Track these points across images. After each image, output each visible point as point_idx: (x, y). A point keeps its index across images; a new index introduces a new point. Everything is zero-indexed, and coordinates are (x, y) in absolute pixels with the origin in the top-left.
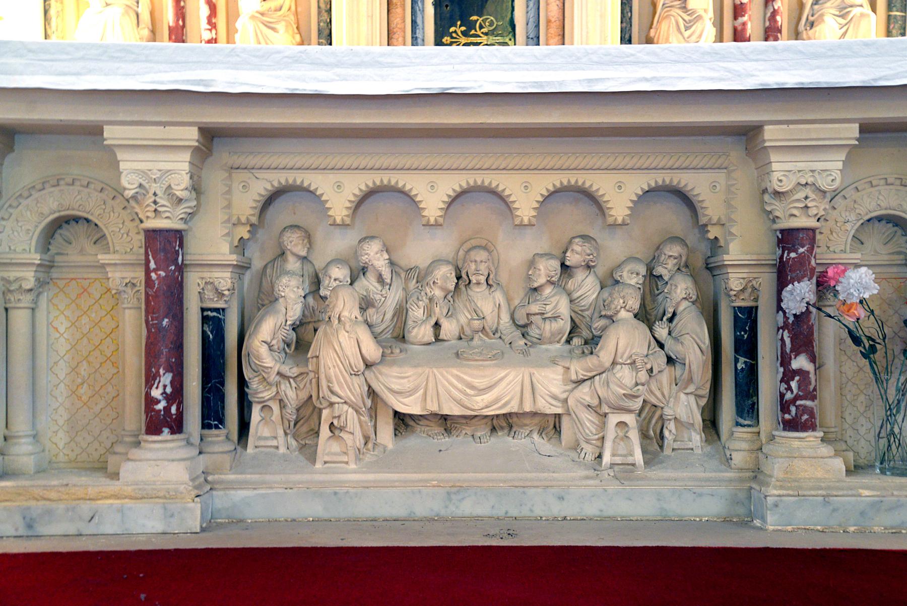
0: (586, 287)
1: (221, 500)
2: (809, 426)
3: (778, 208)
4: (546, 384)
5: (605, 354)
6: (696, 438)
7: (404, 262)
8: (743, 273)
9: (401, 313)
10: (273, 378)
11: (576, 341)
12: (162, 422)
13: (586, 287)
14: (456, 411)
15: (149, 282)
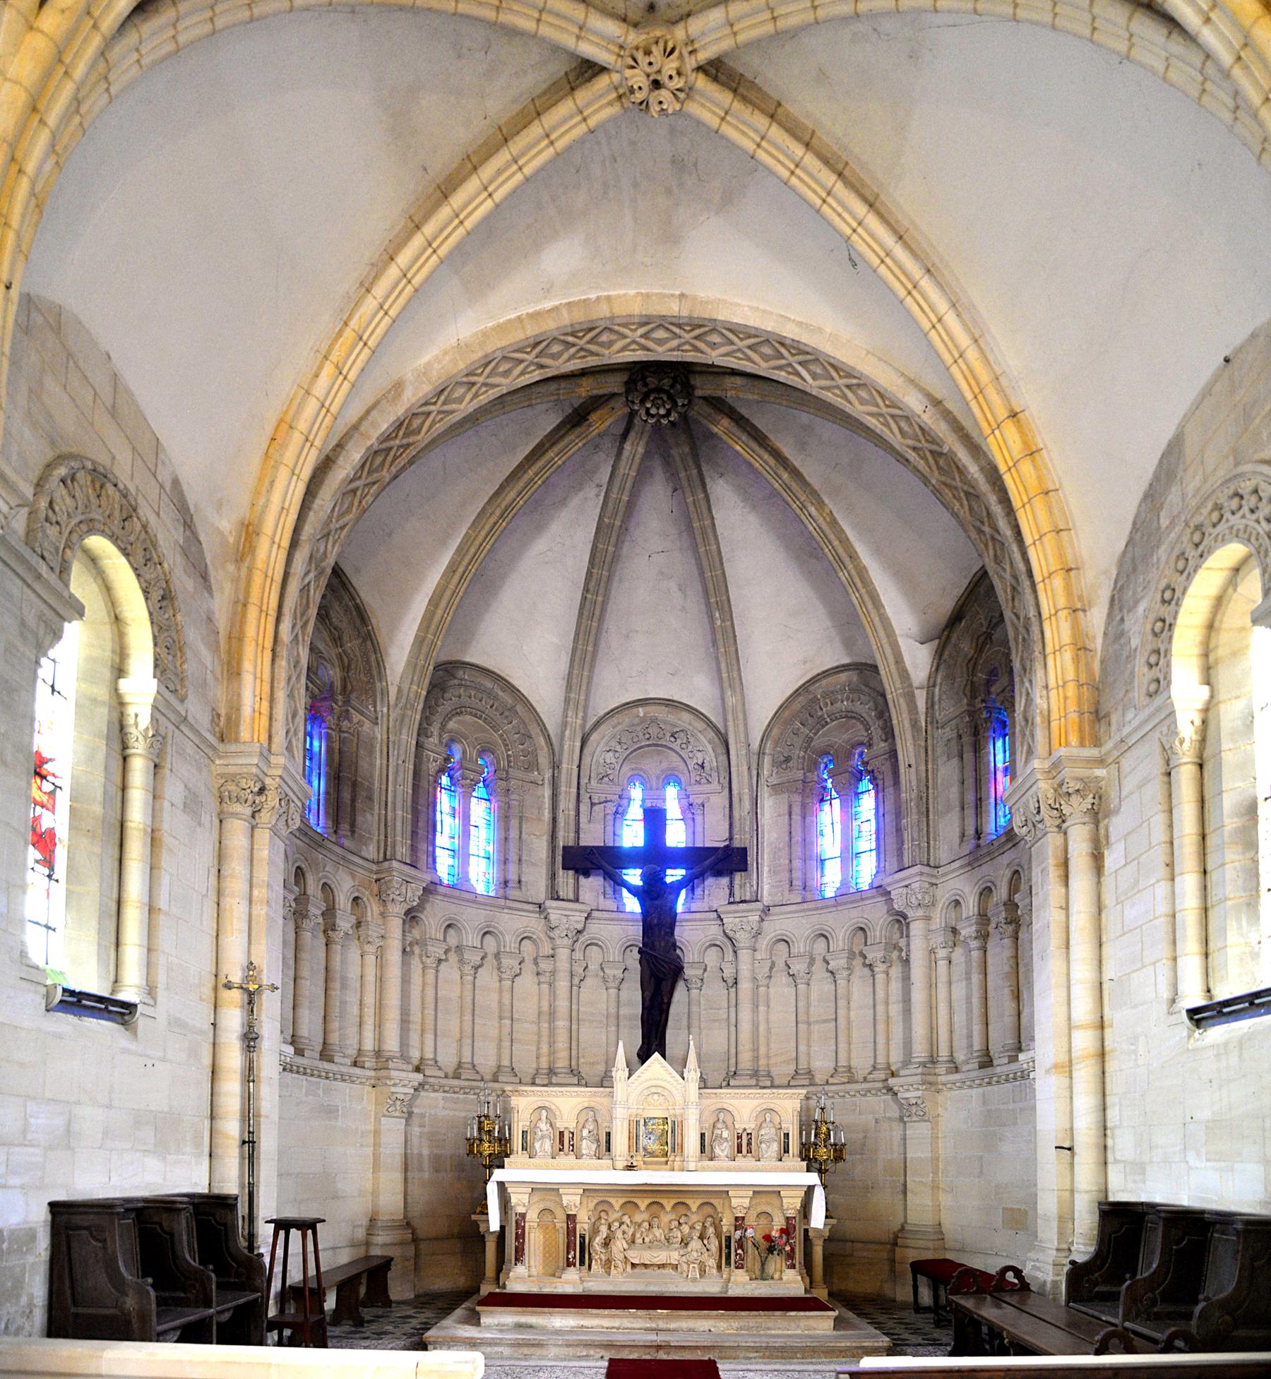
0: (686, 1229)
6: (715, 1271)
13: (686, 1229)
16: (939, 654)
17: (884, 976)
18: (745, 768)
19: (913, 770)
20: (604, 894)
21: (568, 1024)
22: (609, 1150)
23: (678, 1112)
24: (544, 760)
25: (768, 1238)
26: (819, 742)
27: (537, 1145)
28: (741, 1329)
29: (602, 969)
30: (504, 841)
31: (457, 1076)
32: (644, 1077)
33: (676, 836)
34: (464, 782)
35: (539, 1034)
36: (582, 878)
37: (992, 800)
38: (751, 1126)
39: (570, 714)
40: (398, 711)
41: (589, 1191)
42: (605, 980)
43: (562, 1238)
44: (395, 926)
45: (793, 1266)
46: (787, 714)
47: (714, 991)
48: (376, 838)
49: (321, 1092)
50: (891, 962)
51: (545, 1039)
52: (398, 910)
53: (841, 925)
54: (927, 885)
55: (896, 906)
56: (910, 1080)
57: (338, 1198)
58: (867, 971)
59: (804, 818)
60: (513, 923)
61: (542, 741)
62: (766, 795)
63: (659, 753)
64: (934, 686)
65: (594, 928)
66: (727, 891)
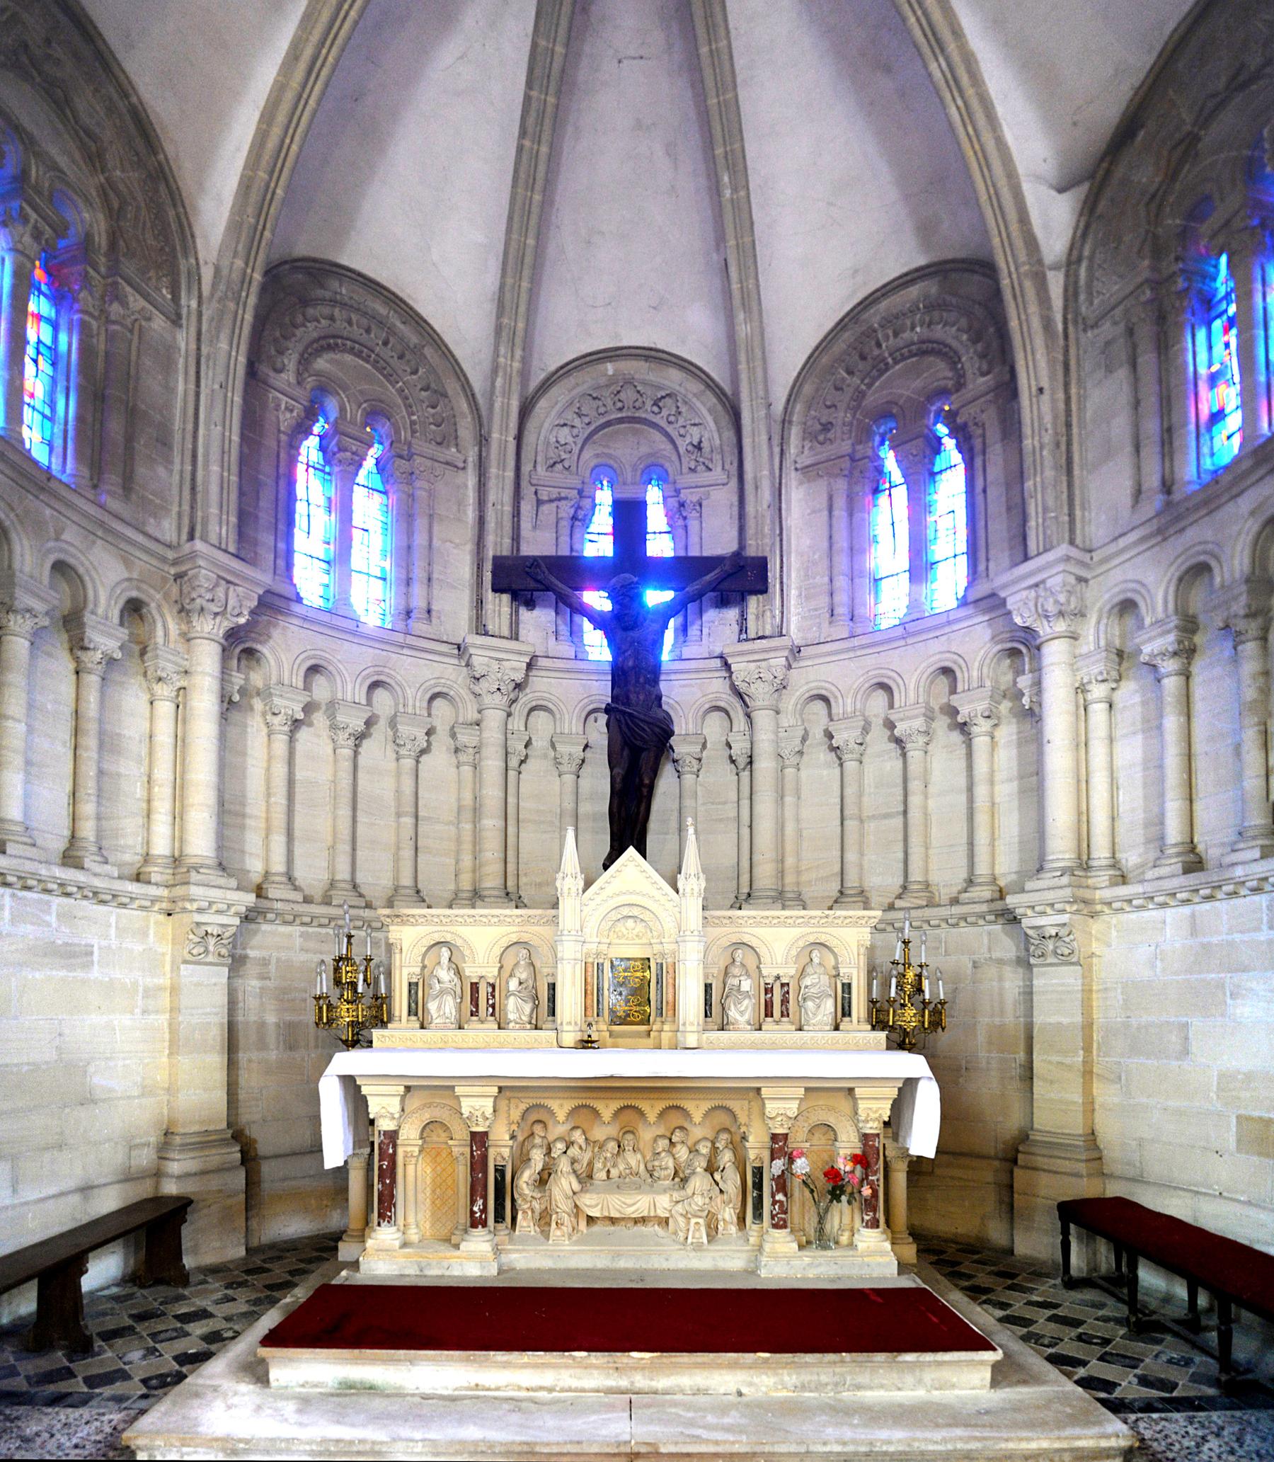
0: (682, 1153)
1: (504, 1258)
2: (785, 1227)
3: (770, 1123)
4: (663, 1203)
5: (689, 1191)
6: (733, 1229)
7: (592, 1139)
8: (756, 1151)
9: (590, 1164)
10: (529, 1199)
11: (677, 1180)
12: (476, 1222)
13: (682, 1153)
14: (617, 1215)
15: (472, 1156)
16: (1089, 212)
17: (988, 739)
18: (764, 437)
19: (1046, 397)
20: (556, 633)
21: (501, 823)
22: (552, 1012)
23: (668, 948)
24: (466, 430)
25: (833, 1174)
26: (873, 398)
27: (432, 1006)
28: (803, 1388)
29: (553, 746)
30: (405, 553)
31: (327, 901)
32: (610, 890)
33: (660, 546)
34: (340, 455)
35: (459, 841)
36: (523, 611)
37: (1192, 427)
38: (788, 972)
39: (502, 350)
40: (215, 305)
41: (507, 1090)
42: (557, 762)
43: (462, 1173)
44: (207, 658)
45: (874, 1224)
46: (825, 360)
47: (719, 776)
48: (175, 509)
49: (52, 919)
50: (999, 718)
51: (467, 847)
52: (210, 628)
53: (912, 669)
54: (1072, 580)
55: (1018, 620)
56: (1050, 896)
57: (94, 1102)
58: (956, 737)
59: (851, 515)
60: (416, 672)
61: (464, 406)
62: (794, 483)
63: (636, 432)
64: (1079, 260)
65: (542, 685)
66: (736, 628)
